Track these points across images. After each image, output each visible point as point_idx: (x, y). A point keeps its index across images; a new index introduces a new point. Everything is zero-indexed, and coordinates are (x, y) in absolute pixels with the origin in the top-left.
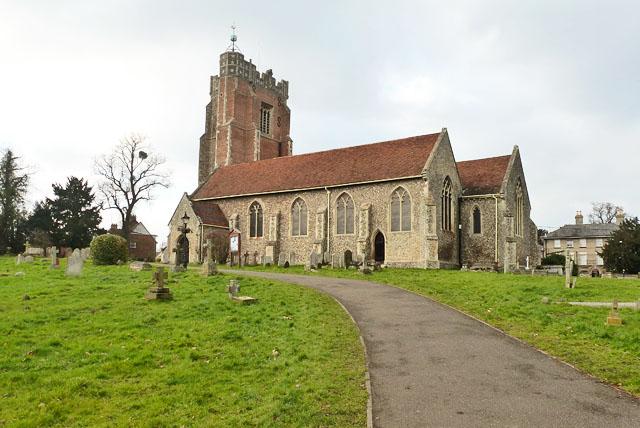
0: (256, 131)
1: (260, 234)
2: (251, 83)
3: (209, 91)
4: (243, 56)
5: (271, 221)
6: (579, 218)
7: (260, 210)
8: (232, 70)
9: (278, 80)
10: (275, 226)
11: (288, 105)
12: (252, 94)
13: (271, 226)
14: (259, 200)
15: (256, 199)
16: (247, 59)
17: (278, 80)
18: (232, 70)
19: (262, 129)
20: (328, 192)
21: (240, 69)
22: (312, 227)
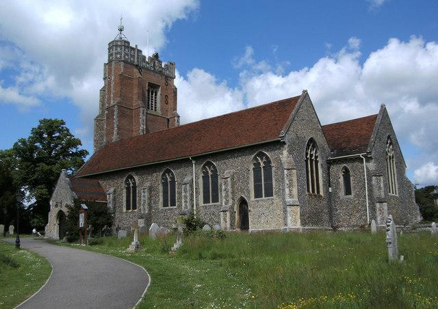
5: (143, 194)
10: (146, 199)
21: (126, 54)
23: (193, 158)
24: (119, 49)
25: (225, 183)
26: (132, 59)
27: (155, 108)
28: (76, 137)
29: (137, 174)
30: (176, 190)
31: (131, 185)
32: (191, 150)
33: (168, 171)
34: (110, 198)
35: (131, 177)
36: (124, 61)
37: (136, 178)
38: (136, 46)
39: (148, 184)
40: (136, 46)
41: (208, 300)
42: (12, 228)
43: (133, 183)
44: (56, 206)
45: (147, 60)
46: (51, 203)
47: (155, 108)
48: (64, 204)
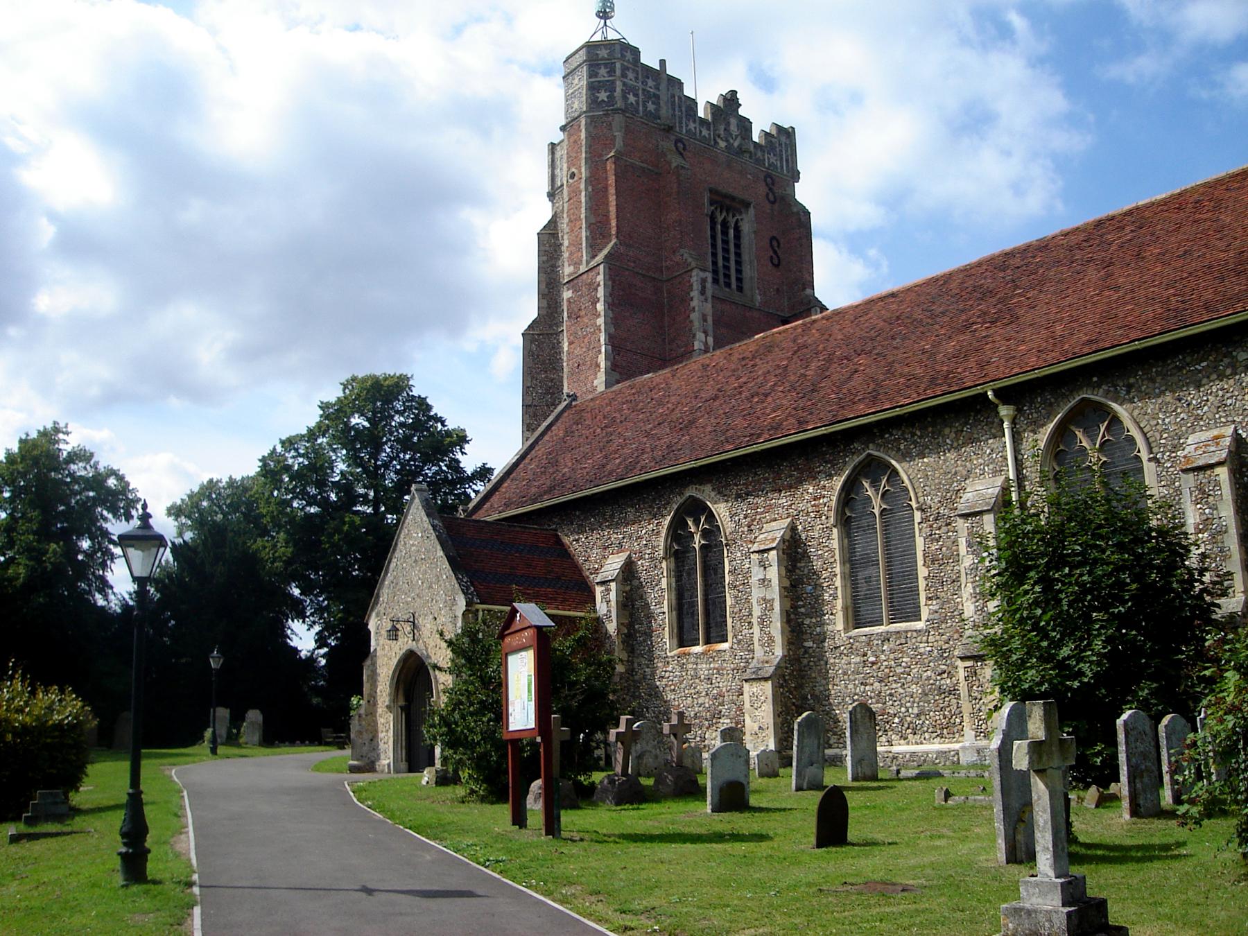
0: (696, 277)
1: (715, 632)
2: (669, 129)
3: (545, 187)
4: (636, 52)
5: (757, 574)
6: (87, 775)
7: (711, 533)
8: (603, 96)
9: (760, 126)
10: (775, 593)
11: (800, 197)
12: (676, 161)
13: (757, 593)
14: (705, 493)
15: (691, 492)
16: (649, 59)
17: (760, 126)
18: (603, 96)
19: (720, 276)
20: (1005, 411)
21: (628, 89)
22: (944, 583)
23: (1005, 395)
24: (603, 71)
25: (1203, 495)
26: (651, 107)
27: (739, 280)
28: (451, 425)
29: (723, 494)
30: (920, 543)
31: (698, 541)
32: (982, 365)
33: (874, 469)
34: (606, 604)
35: (697, 509)
36: (623, 111)
37: (721, 510)
38: (663, 62)
39: (775, 531)
40: (663, 62)
41: (5, 511)
42: (254, 716)
43: (705, 534)
44: (393, 634)
45: (701, 114)
46: (372, 626)
47: (739, 280)
48: (427, 626)
